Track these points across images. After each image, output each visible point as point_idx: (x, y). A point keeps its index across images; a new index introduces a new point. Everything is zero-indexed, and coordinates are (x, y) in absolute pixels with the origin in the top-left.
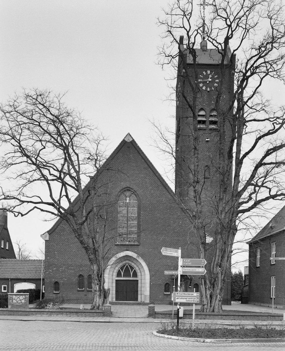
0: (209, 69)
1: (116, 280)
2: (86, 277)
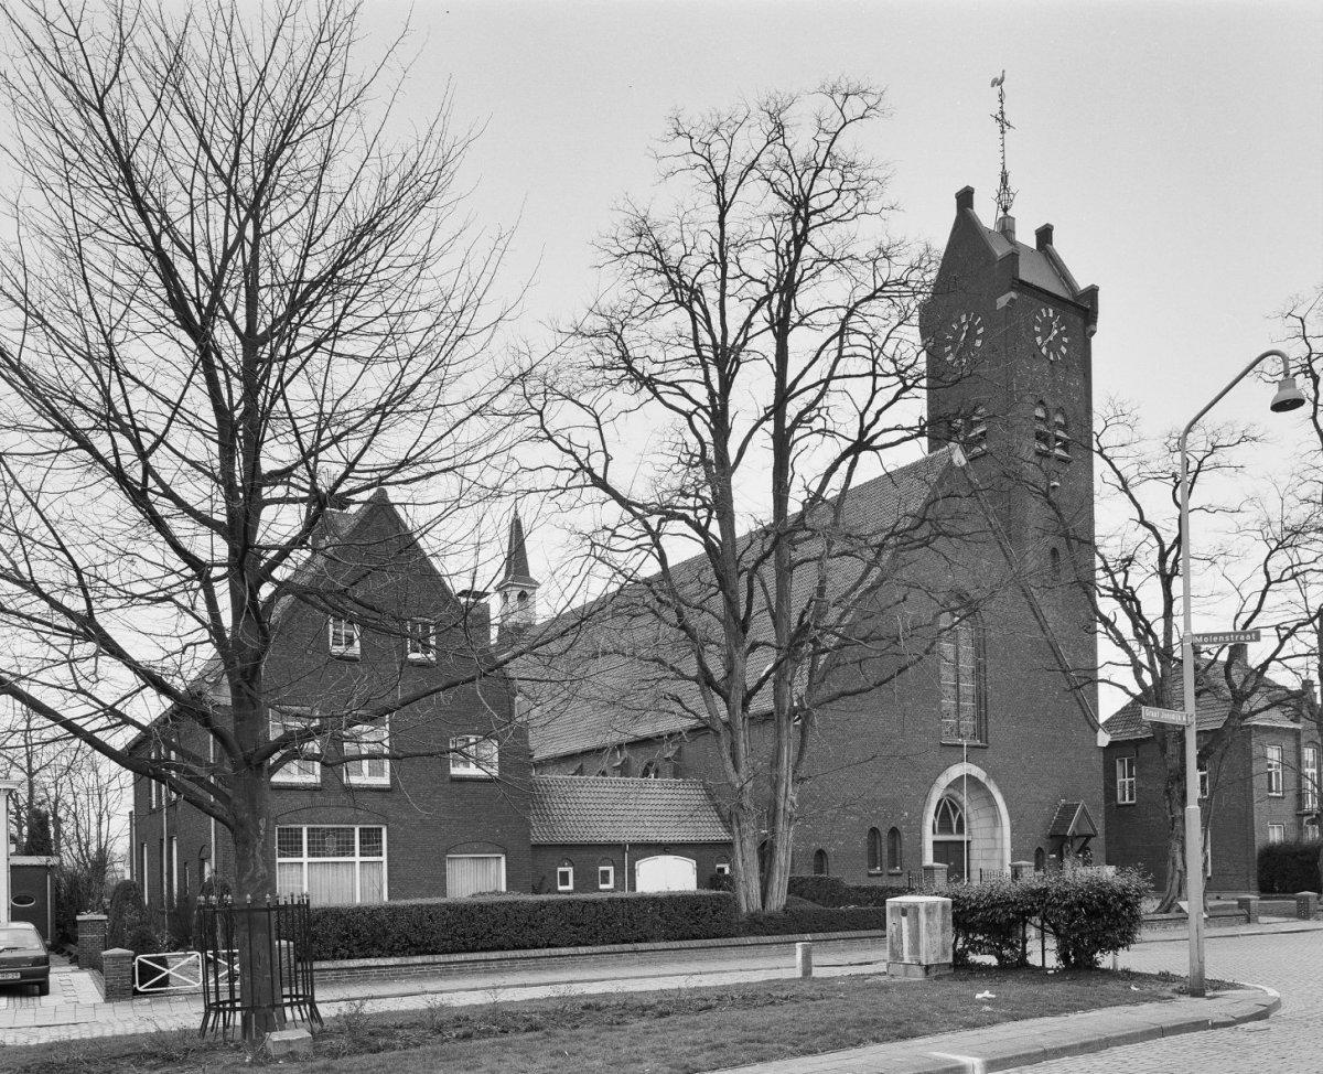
0: (1053, 307)
1: (13, 868)
2: (884, 834)
